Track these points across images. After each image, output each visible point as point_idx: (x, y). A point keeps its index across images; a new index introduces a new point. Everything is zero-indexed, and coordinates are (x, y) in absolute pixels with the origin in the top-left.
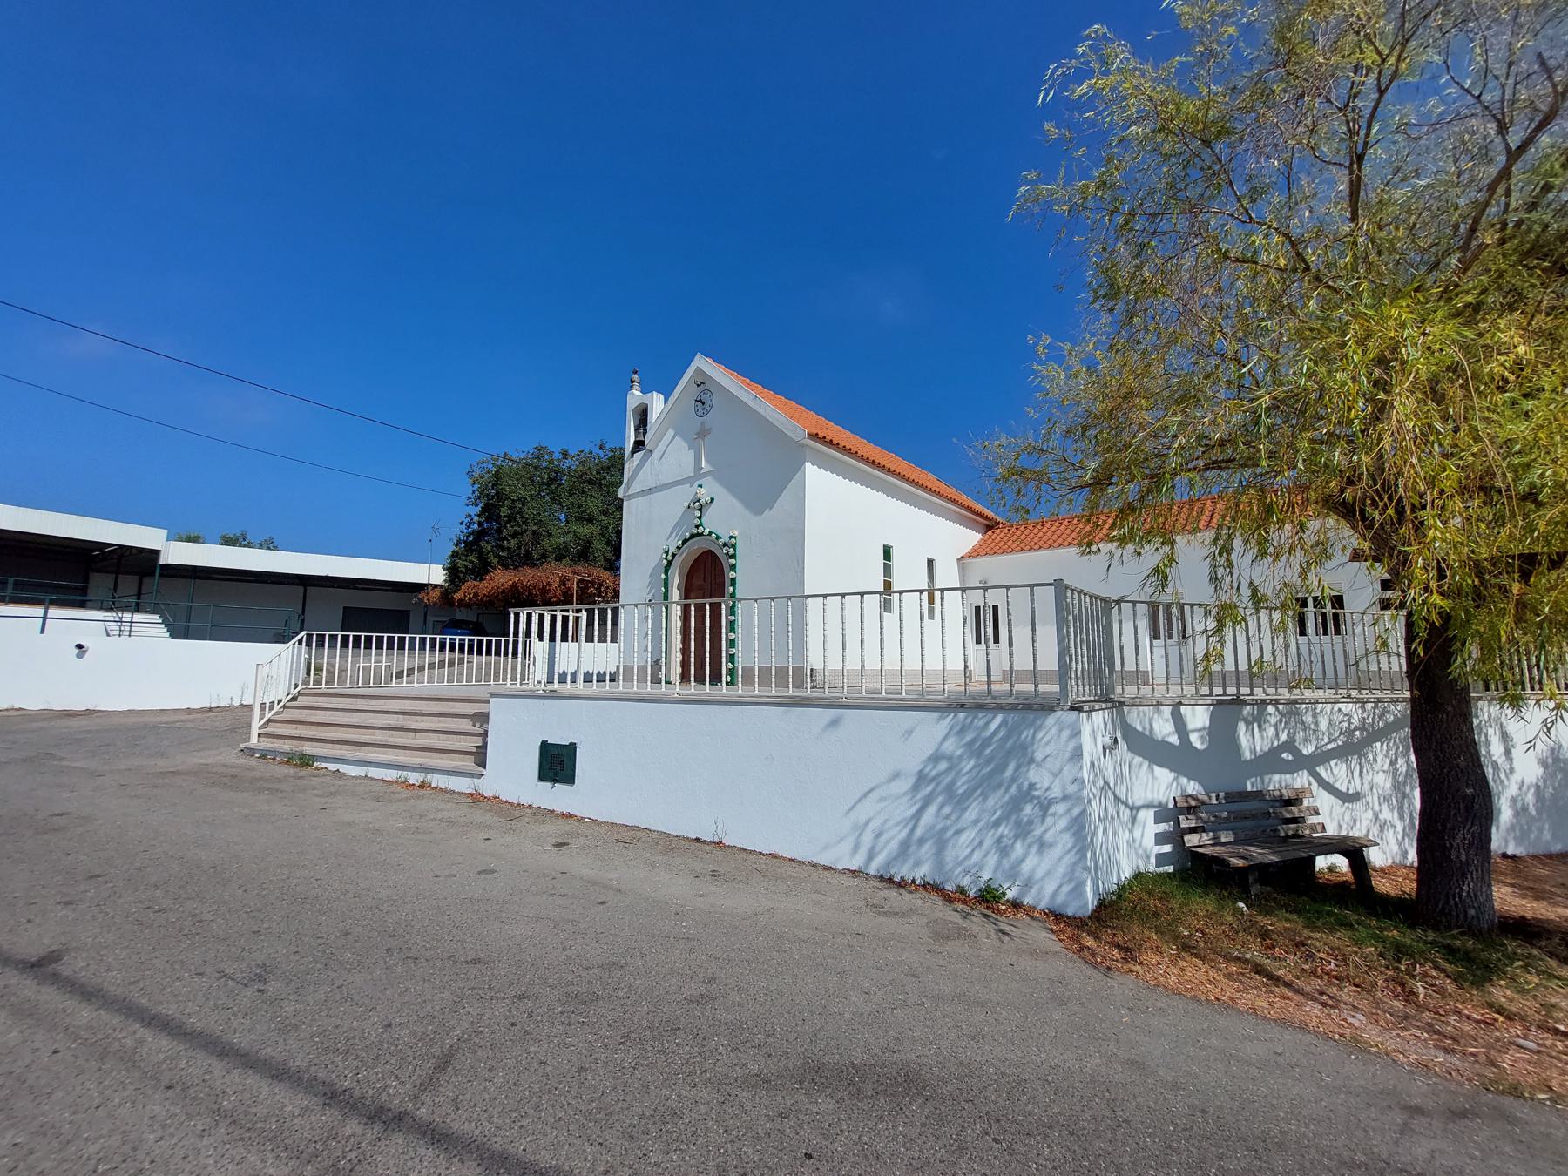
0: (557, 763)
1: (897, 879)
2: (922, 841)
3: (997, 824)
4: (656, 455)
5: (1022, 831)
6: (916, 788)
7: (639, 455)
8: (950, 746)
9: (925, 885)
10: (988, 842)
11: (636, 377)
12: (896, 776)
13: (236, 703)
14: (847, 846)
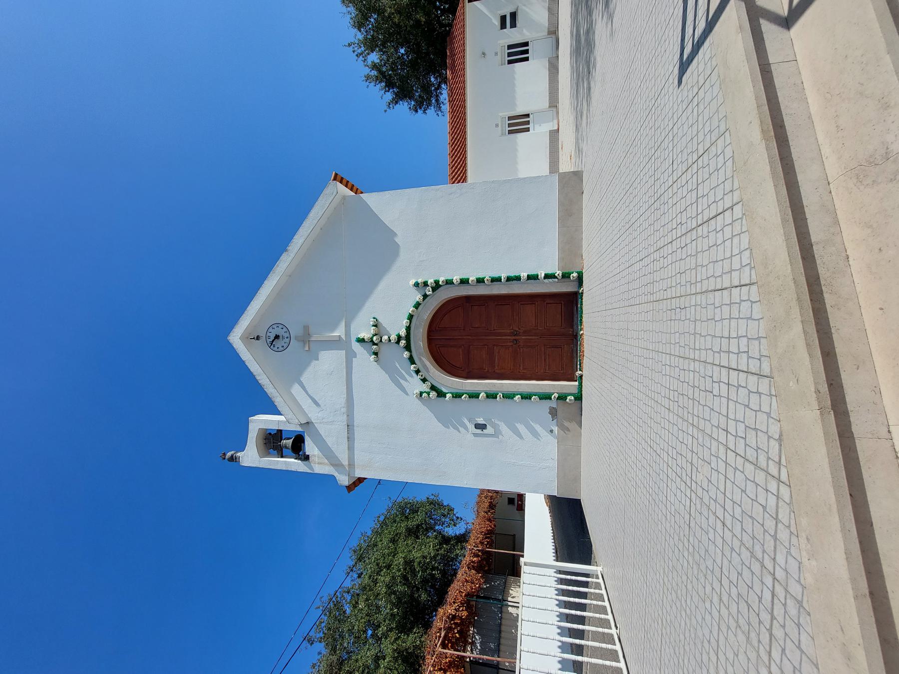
4: (314, 414)
7: (310, 447)
11: (229, 454)
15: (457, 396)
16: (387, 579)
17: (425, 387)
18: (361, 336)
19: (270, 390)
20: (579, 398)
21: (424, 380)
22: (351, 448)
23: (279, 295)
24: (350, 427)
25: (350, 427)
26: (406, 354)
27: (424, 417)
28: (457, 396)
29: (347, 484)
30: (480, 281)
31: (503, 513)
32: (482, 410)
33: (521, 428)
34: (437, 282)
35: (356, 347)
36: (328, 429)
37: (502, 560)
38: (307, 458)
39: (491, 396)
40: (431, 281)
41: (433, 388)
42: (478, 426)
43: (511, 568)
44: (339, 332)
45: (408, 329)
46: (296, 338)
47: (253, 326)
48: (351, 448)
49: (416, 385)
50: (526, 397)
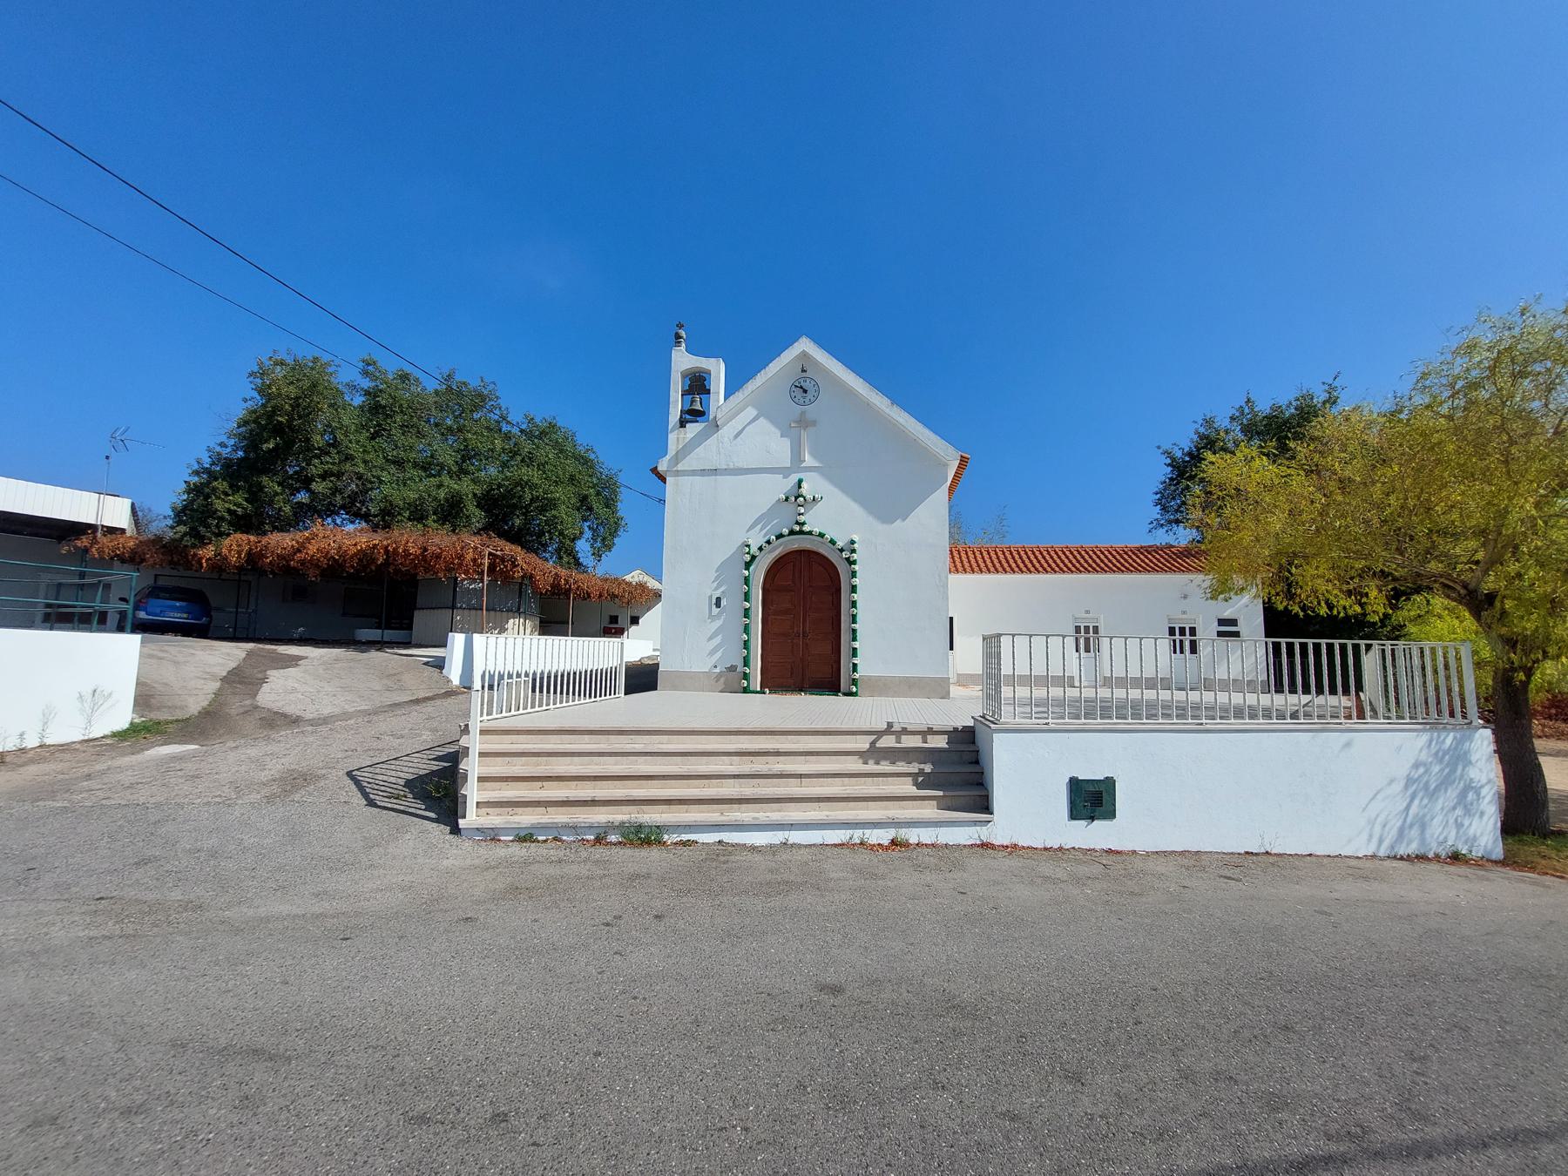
0: (1091, 799)
1: (1431, 855)
2: (1411, 826)
3: (1454, 808)
4: (727, 432)
5: (1468, 812)
6: (1406, 787)
7: (693, 429)
8: (1423, 756)
9: (1417, 857)
10: (1452, 821)
11: (683, 334)
12: (1392, 781)
13: (32, 742)
14: (1365, 836)
15: (746, 581)
16: (536, 480)
17: (754, 550)
18: (804, 485)
19: (751, 386)
20: (745, 690)
21: (760, 549)
22: (694, 473)
23: (851, 393)
24: (715, 472)
25: (715, 472)
26: (785, 531)
27: (725, 550)
28: (746, 581)
29: (660, 469)
30: (854, 604)
31: (612, 613)
32: (733, 603)
33: (718, 640)
34: (854, 562)
35: (794, 478)
36: (710, 452)
37: (556, 613)
38: (683, 424)
39: (747, 613)
40: (855, 556)
41: (753, 557)
42: (719, 599)
43: (551, 624)
44: (809, 460)
45: (810, 533)
46: (803, 413)
47: (816, 363)
48: (694, 473)
49: (756, 541)
50: (746, 645)
